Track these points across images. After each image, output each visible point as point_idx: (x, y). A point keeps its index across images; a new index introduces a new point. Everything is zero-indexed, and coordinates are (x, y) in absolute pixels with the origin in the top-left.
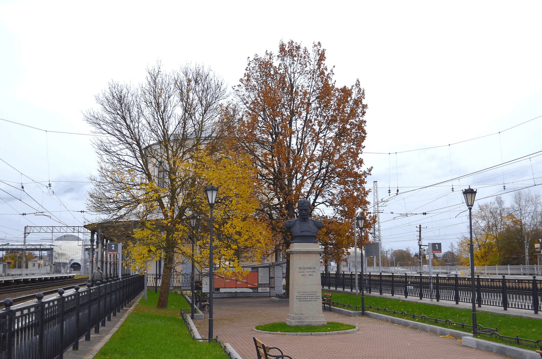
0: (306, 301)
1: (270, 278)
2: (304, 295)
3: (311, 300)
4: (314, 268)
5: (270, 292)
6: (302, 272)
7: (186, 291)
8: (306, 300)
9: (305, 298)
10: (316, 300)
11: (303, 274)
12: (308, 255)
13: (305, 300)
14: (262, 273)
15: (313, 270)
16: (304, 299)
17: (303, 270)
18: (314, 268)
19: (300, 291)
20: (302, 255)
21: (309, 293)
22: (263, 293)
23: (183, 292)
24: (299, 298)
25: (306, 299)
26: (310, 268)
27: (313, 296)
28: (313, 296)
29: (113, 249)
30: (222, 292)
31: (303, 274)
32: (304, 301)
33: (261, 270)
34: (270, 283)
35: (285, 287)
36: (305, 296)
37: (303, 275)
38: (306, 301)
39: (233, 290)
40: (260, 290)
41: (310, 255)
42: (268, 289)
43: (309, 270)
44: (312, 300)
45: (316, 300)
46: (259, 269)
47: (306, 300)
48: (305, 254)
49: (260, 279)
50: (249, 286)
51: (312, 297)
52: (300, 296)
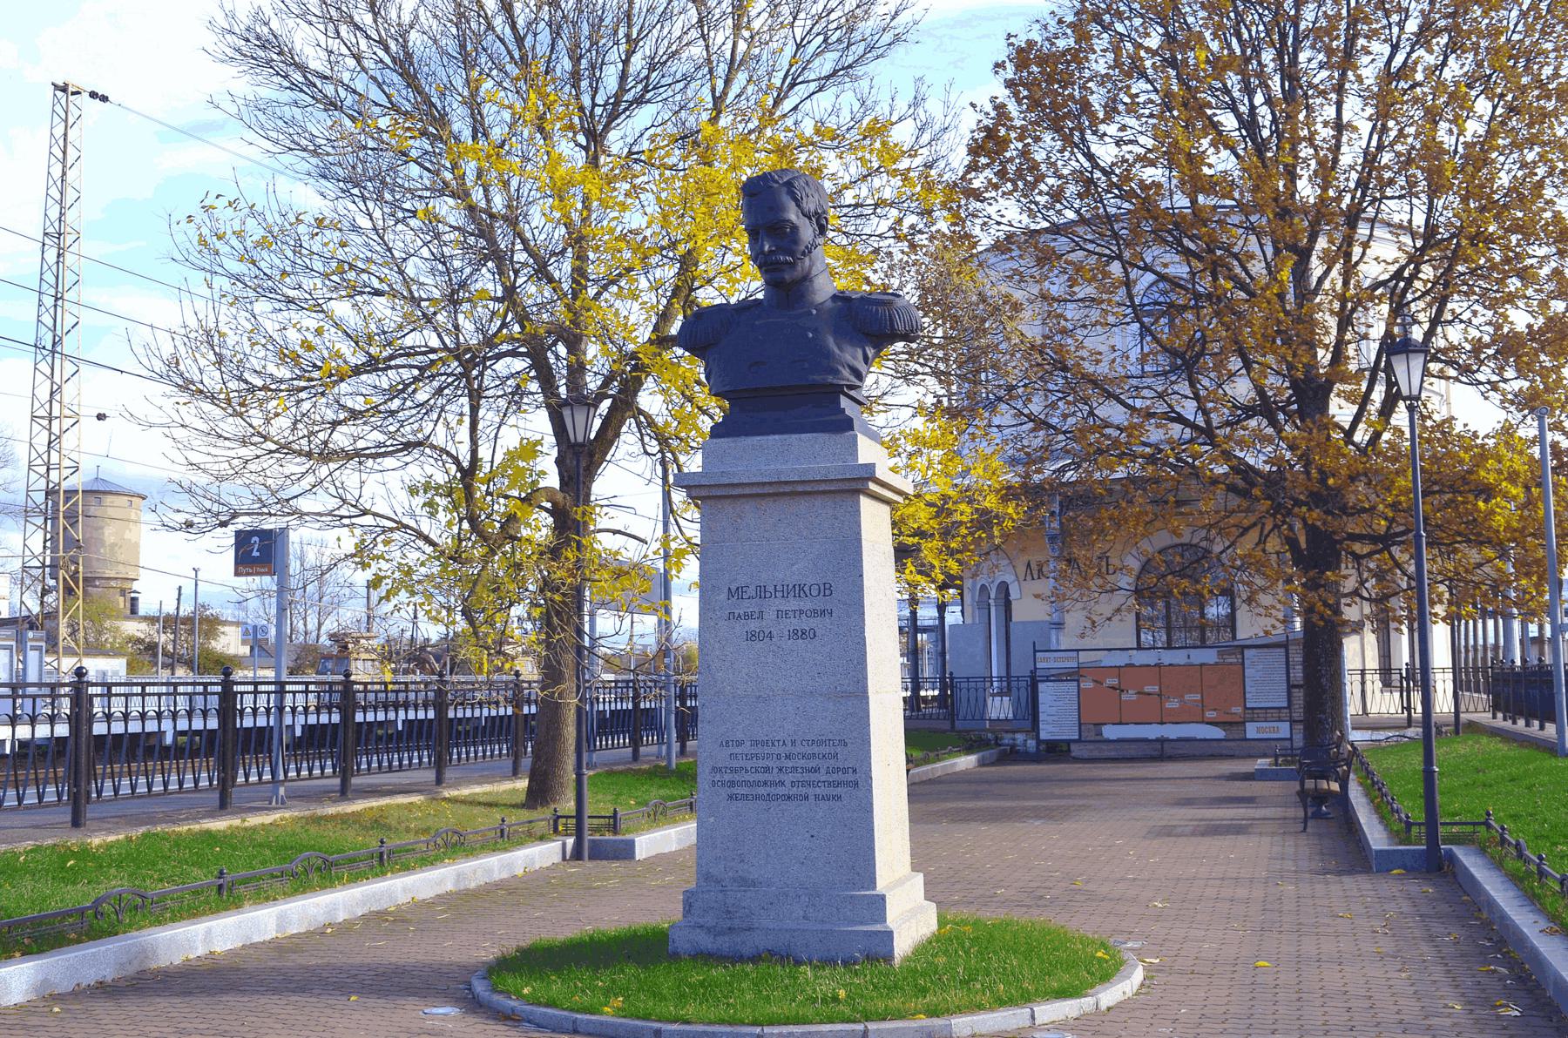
2: (761, 763)
3: (803, 791)
5: (1291, 739)
6: (748, 616)
7: (1010, 736)
8: (773, 790)
9: (813, 777)
11: (753, 625)
13: (762, 791)
15: (819, 604)
16: (757, 784)
19: (740, 736)
20: (748, 507)
21: (789, 748)
23: (1002, 739)
24: (727, 777)
26: (799, 590)
27: (816, 770)
28: (816, 770)
30: (1113, 737)
31: (753, 625)
32: (757, 797)
33: (1255, 659)
36: (767, 770)
37: (752, 636)
39: (1152, 732)
40: (1252, 731)
41: (803, 505)
43: (793, 604)
44: (811, 791)
46: (1246, 652)
47: (773, 790)
49: (1253, 689)
50: (1210, 715)
51: (813, 777)
52: (735, 764)
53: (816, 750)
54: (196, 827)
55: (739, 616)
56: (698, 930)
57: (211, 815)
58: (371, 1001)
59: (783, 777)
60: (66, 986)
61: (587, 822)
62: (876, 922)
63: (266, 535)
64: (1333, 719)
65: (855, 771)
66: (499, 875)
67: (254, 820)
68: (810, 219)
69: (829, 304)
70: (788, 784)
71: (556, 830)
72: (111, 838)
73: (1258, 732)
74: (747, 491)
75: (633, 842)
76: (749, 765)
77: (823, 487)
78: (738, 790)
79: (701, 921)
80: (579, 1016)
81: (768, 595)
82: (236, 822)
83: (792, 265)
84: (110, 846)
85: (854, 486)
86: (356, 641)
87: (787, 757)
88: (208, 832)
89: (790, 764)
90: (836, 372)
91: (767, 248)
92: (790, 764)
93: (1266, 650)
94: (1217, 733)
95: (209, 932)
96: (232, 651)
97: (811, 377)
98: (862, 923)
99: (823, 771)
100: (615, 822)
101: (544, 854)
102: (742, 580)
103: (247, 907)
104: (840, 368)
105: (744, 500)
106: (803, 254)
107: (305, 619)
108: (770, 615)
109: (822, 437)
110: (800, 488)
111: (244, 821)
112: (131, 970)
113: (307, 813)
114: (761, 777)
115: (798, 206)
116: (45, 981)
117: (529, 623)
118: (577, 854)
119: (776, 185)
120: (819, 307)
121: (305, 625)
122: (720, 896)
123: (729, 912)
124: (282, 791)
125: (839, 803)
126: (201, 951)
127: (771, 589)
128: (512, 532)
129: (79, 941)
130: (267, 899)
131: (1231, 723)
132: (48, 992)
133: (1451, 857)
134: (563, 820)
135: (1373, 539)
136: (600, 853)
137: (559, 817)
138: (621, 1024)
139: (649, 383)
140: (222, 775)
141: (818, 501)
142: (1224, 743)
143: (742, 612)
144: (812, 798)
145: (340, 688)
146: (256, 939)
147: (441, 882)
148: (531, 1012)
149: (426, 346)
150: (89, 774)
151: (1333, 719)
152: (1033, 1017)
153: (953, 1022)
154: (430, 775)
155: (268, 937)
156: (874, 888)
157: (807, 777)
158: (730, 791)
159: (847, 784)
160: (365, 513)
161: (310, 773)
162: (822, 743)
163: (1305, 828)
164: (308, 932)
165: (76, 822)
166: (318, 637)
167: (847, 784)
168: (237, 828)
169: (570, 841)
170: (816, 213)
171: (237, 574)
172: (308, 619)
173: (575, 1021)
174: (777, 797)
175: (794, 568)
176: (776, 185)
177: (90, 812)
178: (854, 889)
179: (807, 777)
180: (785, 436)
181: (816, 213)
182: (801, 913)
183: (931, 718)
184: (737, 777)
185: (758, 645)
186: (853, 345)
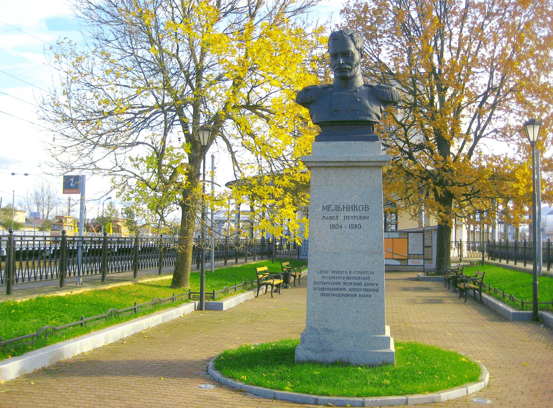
0: (339, 295)
1: (424, 247)
2: (336, 281)
4: (366, 208)
5: (424, 266)
6: (331, 218)
8: (341, 292)
9: (358, 287)
10: (367, 293)
11: (334, 222)
12: (348, 171)
13: (336, 292)
14: (414, 240)
15: (363, 213)
16: (334, 289)
17: (333, 214)
18: (366, 208)
19: (326, 269)
20: (332, 172)
21: (348, 275)
22: (413, 267)
24: (321, 286)
25: (341, 289)
26: (354, 208)
27: (360, 284)
28: (360, 284)
29: (72, 185)
31: (334, 222)
32: (334, 295)
34: (423, 254)
35: (260, 256)
36: (338, 283)
37: (333, 227)
38: (339, 295)
41: (356, 172)
42: (421, 262)
43: (351, 213)
44: (358, 293)
45: (367, 293)
46: (409, 234)
47: (341, 292)
48: (340, 170)
50: (396, 257)
51: (358, 287)
52: (325, 281)
53: (360, 276)
54: (55, 295)
55: (327, 218)
56: (308, 351)
57: (57, 290)
58: (172, 381)
59: (345, 287)
60: (30, 371)
61: (204, 295)
62: (386, 348)
63: (77, 178)
64: (447, 259)
65: (377, 285)
66: (176, 316)
67: (75, 292)
68: (359, 51)
69: (363, 88)
70: (347, 290)
71: (190, 298)
72: (24, 300)
73: (412, 263)
74: (333, 165)
75: (222, 304)
76: (330, 281)
77: (366, 164)
78: (324, 292)
79: (309, 347)
80: (277, 391)
81: (340, 209)
82: (69, 293)
83: (351, 70)
84: (25, 303)
85: (380, 164)
86: (66, 219)
87: (348, 278)
88: (59, 297)
89: (349, 281)
90: (370, 116)
91: (341, 62)
92: (349, 281)
93: (415, 234)
94: (398, 263)
95: (82, 344)
96: (19, 221)
97: (360, 118)
98: (379, 349)
99: (363, 284)
100: (214, 295)
101: (188, 308)
102: (329, 203)
103: (92, 332)
104: (372, 114)
105: (331, 168)
106: (356, 65)
107: (43, 210)
108: (341, 218)
109: (365, 143)
110: (357, 164)
111: (72, 292)
112: (54, 362)
113: (93, 289)
114: (336, 286)
115: (355, 45)
116: (23, 369)
117: (125, 214)
118: (200, 308)
119: (346, 36)
120: (359, 88)
121: (43, 213)
122: (317, 336)
123: (321, 343)
124: (81, 279)
125: (370, 298)
126: (78, 352)
127: (342, 207)
128: (174, 180)
129: (32, 350)
130: (99, 329)
131: (401, 259)
132: (24, 373)
133: (541, 315)
134: (193, 294)
135: (466, 195)
136: (210, 308)
137: (191, 293)
138: (298, 396)
139: (428, 102)
140: (61, 273)
141: (363, 170)
142: (399, 267)
143: (328, 216)
144: (358, 296)
145: (103, 239)
146: (98, 346)
147: (158, 320)
148: (251, 388)
149: (141, 104)
150: (13, 274)
151: (447, 259)
152: (467, 392)
153: (441, 394)
154: (132, 273)
155: (101, 345)
156: (384, 334)
157: (356, 287)
158: (321, 292)
159: (373, 290)
160: (122, 170)
161: (96, 273)
162: (362, 273)
163: (465, 302)
164: (115, 342)
165: (8, 292)
166: (48, 217)
167: (373, 290)
168: (70, 295)
169: (197, 303)
170: (361, 49)
171: (63, 193)
172: (44, 210)
173: (275, 394)
174: (343, 295)
175: (352, 198)
176: (346, 36)
177: (14, 288)
178: (375, 334)
179: (356, 287)
180: (349, 142)
181: (361, 49)
182: (353, 344)
183: (280, 254)
184: (325, 286)
185: (335, 230)
186: (376, 105)
